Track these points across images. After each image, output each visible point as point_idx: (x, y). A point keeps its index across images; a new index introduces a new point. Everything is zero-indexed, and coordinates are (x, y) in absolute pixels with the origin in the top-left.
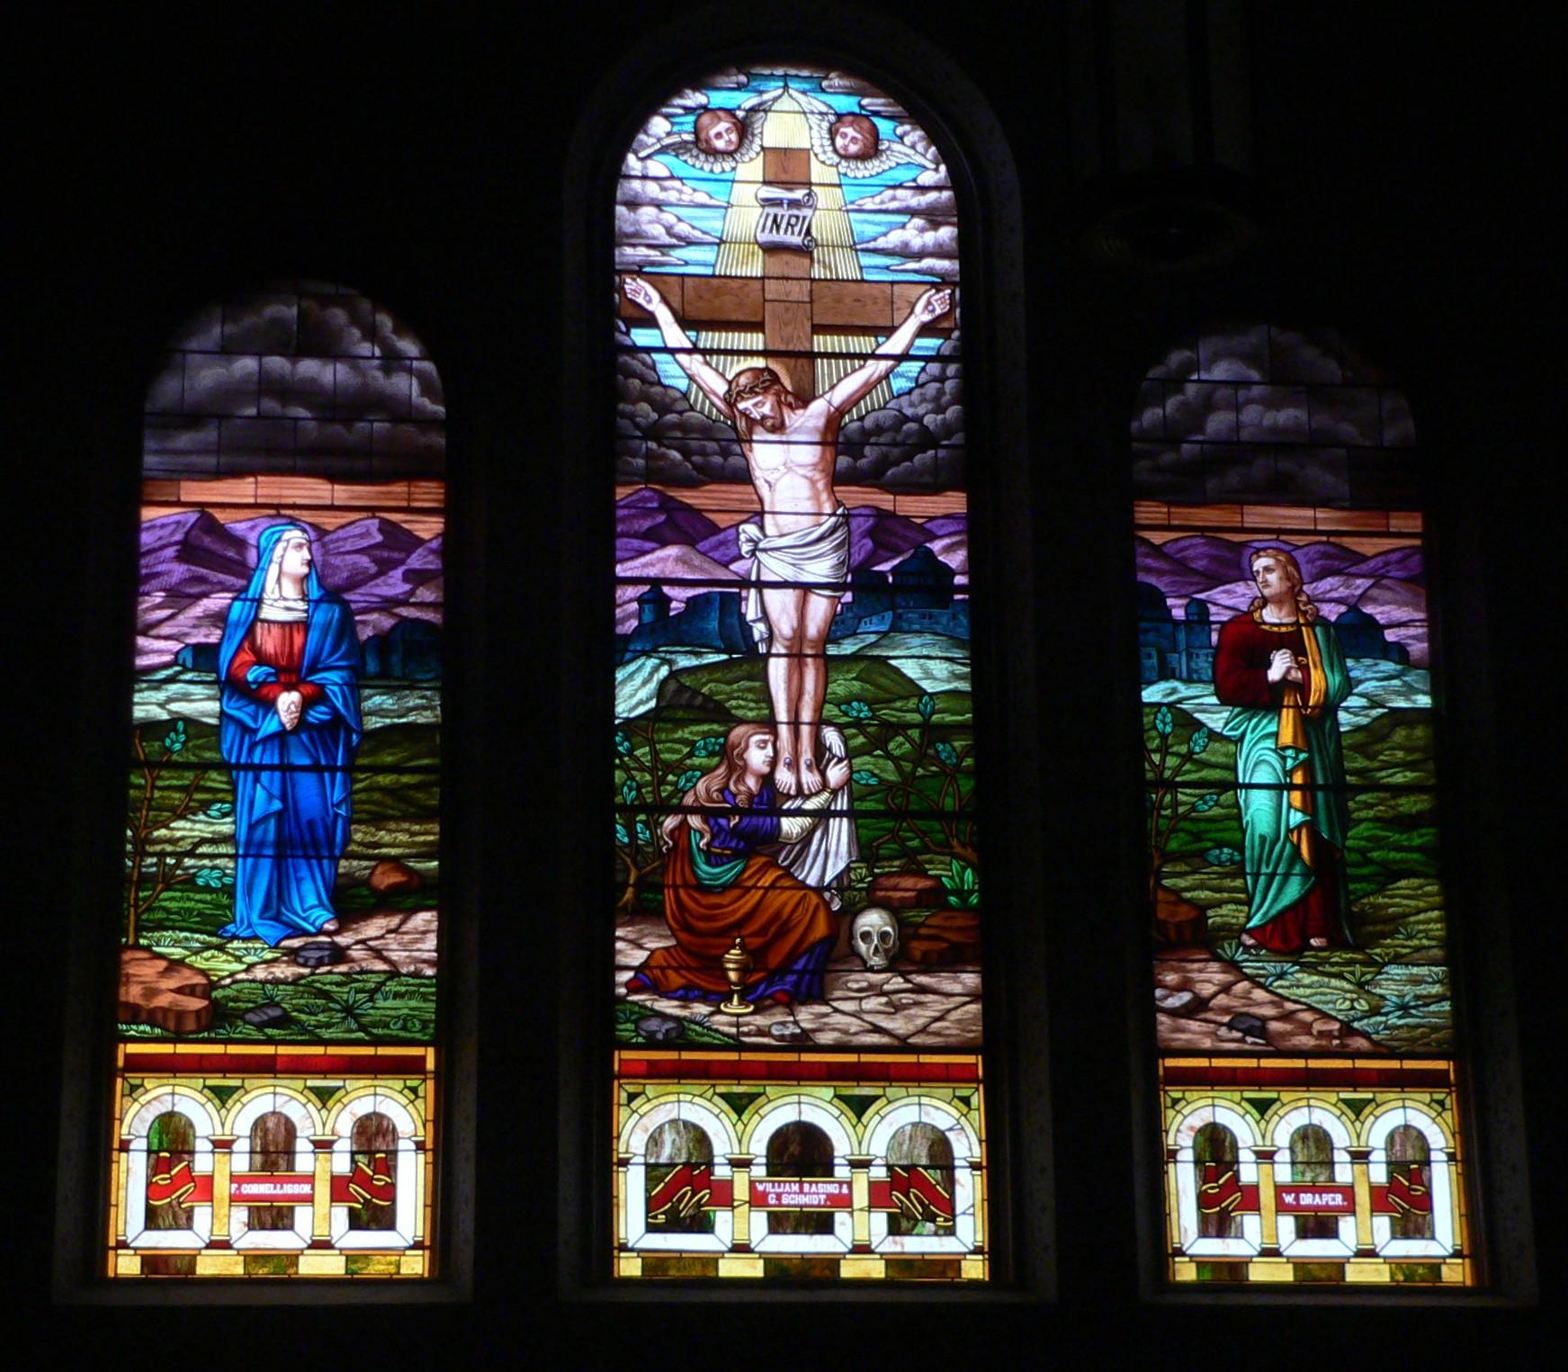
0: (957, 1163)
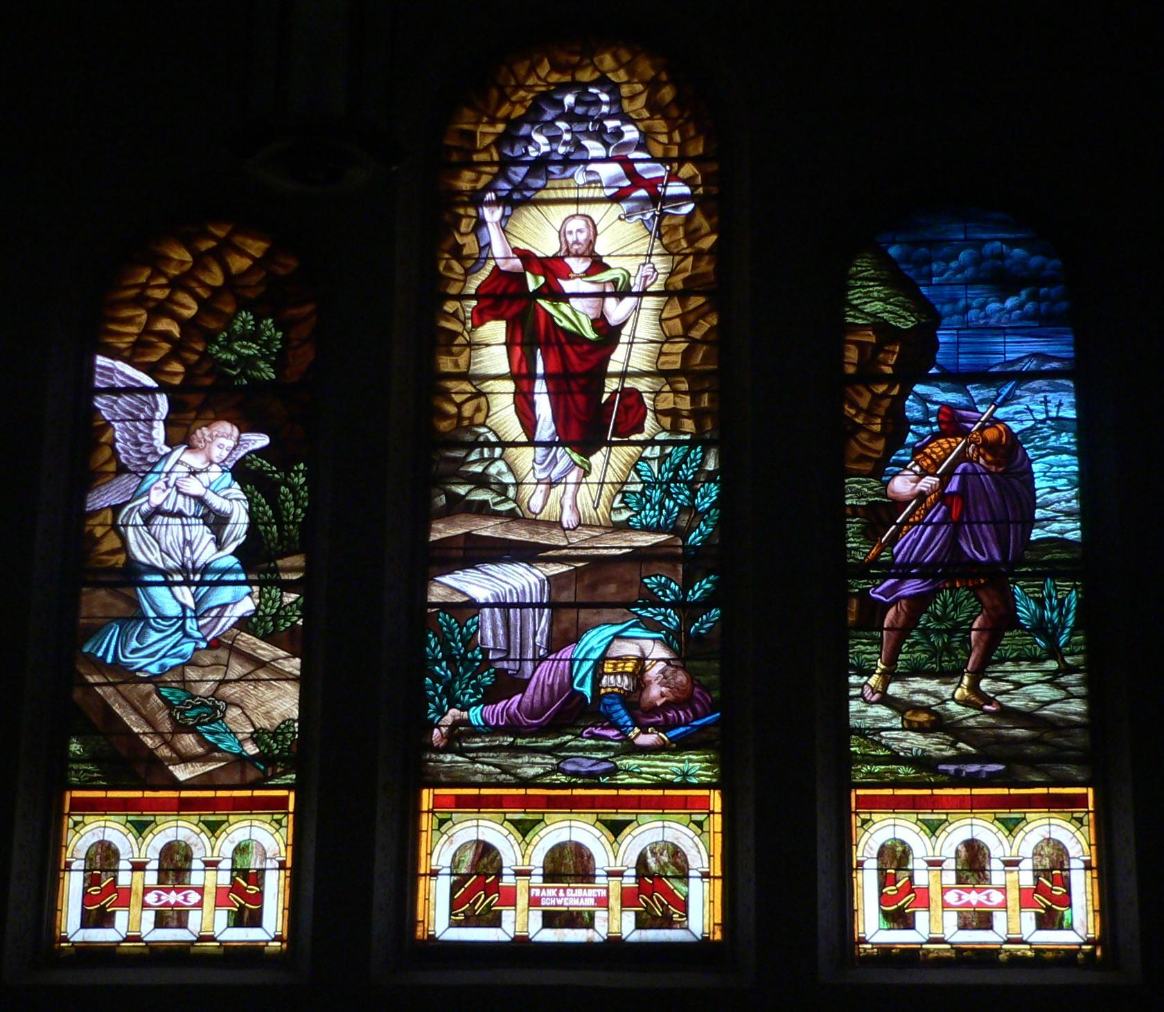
0: (597, 872)
